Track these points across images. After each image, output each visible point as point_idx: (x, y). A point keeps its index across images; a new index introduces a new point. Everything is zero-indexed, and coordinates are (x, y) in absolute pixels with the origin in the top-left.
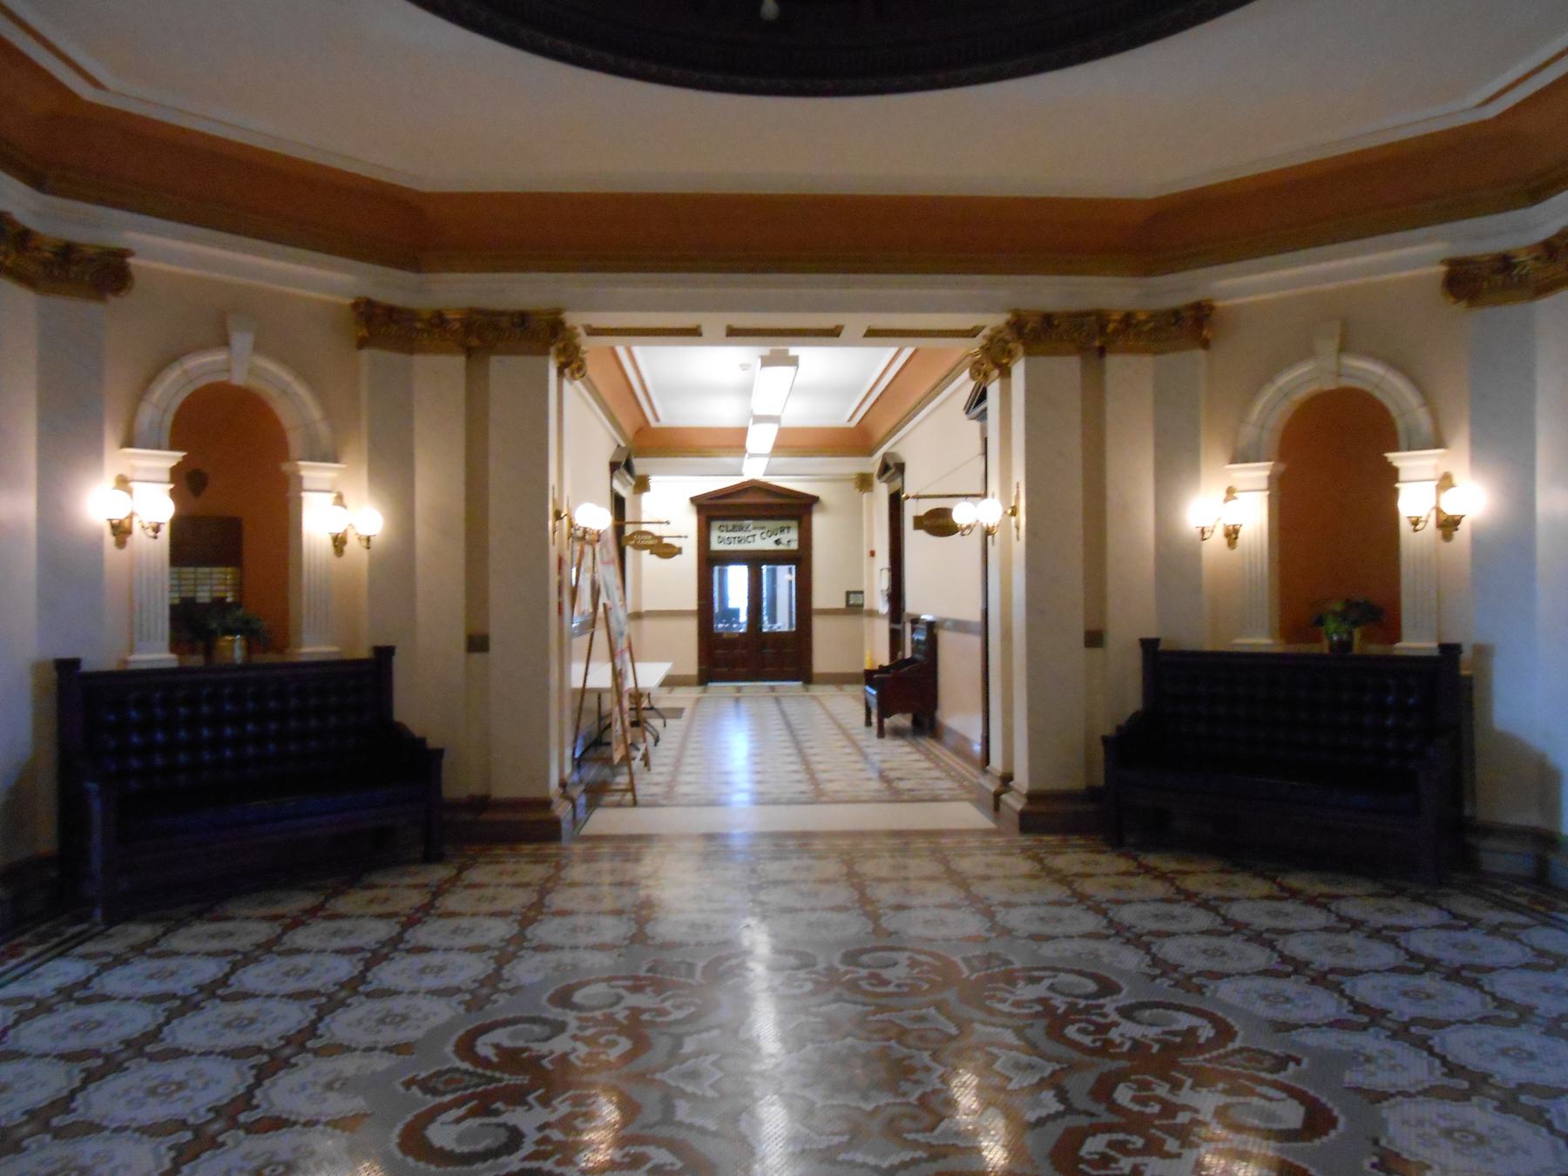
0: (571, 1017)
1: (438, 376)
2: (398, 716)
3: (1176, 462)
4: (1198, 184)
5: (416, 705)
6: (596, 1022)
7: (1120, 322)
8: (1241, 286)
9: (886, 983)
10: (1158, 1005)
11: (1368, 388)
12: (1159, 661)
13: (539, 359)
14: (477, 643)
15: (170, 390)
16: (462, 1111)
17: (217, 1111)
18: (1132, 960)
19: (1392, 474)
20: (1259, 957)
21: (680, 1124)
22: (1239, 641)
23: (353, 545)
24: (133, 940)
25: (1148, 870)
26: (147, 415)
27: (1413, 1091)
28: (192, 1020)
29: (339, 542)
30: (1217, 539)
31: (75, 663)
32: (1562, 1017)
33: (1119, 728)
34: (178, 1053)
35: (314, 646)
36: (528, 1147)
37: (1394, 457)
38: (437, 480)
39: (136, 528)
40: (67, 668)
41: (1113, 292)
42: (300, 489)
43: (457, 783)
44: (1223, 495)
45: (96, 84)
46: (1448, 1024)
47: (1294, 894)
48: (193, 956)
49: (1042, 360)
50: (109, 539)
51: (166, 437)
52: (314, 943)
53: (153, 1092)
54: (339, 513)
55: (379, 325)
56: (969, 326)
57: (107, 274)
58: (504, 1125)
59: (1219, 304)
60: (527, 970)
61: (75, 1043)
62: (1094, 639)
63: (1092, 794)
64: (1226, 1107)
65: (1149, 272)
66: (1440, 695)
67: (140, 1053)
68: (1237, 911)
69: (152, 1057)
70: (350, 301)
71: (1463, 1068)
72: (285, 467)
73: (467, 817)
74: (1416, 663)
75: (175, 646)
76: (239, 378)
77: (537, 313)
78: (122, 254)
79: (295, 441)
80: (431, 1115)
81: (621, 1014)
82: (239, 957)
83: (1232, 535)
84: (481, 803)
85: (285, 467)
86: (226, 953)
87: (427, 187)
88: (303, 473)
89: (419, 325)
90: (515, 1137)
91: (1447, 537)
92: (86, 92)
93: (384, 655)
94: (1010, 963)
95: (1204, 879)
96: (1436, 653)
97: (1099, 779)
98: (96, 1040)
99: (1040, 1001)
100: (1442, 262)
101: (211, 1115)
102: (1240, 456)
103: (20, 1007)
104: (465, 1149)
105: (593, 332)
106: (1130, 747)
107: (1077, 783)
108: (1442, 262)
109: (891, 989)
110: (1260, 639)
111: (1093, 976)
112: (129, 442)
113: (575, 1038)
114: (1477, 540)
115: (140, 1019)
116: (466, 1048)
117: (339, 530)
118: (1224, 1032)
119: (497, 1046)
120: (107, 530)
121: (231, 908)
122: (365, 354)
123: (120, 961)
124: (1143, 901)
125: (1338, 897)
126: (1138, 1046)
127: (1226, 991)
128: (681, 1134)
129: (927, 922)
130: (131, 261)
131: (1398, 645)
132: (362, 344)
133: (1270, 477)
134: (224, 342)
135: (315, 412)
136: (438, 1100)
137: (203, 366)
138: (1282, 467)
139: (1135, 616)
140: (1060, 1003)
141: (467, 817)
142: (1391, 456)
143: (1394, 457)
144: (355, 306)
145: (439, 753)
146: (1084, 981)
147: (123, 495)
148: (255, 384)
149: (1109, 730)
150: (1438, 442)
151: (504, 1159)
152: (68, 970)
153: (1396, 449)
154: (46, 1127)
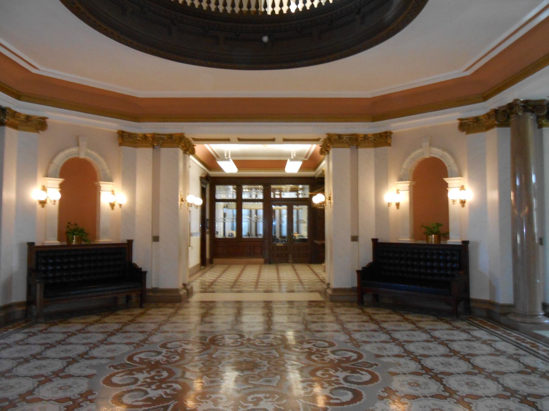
0: (164, 351)
1: (144, 154)
2: (135, 261)
3: (381, 182)
5: (139, 258)
6: (171, 352)
8: (397, 126)
9: (264, 343)
10: (345, 350)
12: (379, 247)
14: (156, 239)
15: (60, 160)
16: (123, 374)
17: (81, 395)
18: (343, 337)
19: (446, 185)
20: (442, 350)
21: (186, 378)
22: (401, 240)
23: (117, 207)
24: (40, 329)
25: (407, 320)
26: (52, 168)
27: (490, 395)
28: (76, 365)
29: (112, 205)
30: (393, 206)
31: (33, 243)
32: (547, 372)
33: (363, 268)
34: (70, 376)
35: (104, 239)
36: (139, 383)
37: (447, 180)
38: (143, 188)
39: (48, 201)
40: (31, 245)
42: (100, 190)
43: (151, 283)
44: (395, 191)
46: (505, 373)
47: (458, 328)
48: (58, 332)
50: (39, 206)
51: (58, 175)
52: (118, 341)
53: (60, 388)
54: (113, 196)
55: (125, 139)
58: (134, 378)
60: (157, 338)
61: (36, 372)
62: (355, 239)
64: (347, 376)
66: (459, 257)
67: (58, 376)
68: (437, 334)
69: (61, 377)
70: (116, 131)
71: (509, 388)
72: (96, 183)
73: (151, 294)
74: (454, 247)
75: (59, 239)
76: (82, 156)
77: (175, 134)
78: (44, 118)
80: (114, 375)
81: (179, 350)
82: (92, 345)
83: (398, 205)
84: (155, 290)
85: (96, 183)
86: (88, 344)
88: (101, 185)
89: (138, 138)
90: (137, 380)
91: (463, 206)
93: (130, 243)
94: (305, 338)
95: (427, 323)
96: (461, 244)
97: (355, 284)
98: (43, 372)
99: (309, 349)
101: (79, 396)
102: (401, 179)
103: (18, 361)
104: (121, 383)
105: (195, 140)
106: (366, 275)
107: (348, 286)
109: (265, 345)
110: (406, 239)
112: (47, 176)
113: (164, 356)
114: (471, 208)
115: (58, 365)
116: (130, 358)
117: (112, 202)
118: (360, 356)
119: (140, 358)
120: (38, 203)
121: (72, 320)
125: (419, 321)
126: (332, 361)
127: (368, 347)
128: (186, 381)
130: (47, 120)
132: (121, 144)
133: (410, 186)
135: (106, 167)
136: (117, 371)
137: (70, 152)
139: (369, 232)
140: (314, 349)
141: (151, 294)
142: (445, 179)
143: (447, 180)
145: (145, 273)
147: (44, 192)
149: (360, 269)
150: (460, 175)
151: (131, 386)
152: (19, 336)
153: (447, 177)
154: (24, 400)
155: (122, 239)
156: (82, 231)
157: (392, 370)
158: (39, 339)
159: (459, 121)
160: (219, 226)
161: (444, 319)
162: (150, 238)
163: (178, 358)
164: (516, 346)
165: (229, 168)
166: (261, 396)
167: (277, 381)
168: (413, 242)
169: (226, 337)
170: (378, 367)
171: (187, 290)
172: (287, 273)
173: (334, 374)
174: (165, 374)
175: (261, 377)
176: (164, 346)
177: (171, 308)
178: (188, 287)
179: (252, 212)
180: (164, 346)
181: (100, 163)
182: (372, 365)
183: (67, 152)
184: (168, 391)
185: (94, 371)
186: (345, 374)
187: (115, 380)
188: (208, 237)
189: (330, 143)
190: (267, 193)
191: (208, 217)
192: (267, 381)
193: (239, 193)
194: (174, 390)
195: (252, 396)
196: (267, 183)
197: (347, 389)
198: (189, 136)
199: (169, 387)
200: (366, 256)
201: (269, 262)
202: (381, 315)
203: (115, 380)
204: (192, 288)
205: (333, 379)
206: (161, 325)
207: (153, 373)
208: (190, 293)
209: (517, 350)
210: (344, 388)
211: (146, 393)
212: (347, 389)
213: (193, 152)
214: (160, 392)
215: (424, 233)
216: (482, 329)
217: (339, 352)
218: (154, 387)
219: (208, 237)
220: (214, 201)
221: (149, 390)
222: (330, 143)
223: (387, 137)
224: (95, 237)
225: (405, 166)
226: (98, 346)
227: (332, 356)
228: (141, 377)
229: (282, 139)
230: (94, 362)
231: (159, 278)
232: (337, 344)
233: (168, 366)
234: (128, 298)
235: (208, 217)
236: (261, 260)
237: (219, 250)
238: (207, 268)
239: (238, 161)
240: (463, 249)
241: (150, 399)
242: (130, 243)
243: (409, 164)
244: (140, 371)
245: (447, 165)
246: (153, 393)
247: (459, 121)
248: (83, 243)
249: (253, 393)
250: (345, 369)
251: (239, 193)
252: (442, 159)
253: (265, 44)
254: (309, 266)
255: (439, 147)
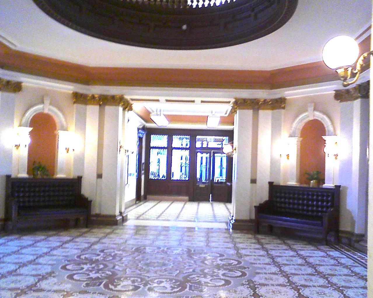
0: (102, 254)
1: (92, 110)
4: (281, 68)
5: (86, 190)
7: (263, 101)
8: (291, 94)
11: (320, 119)
13: (116, 107)
14: (100, 176)
18: (232, 252)
22: (289, 183)
35: (60, 175)
36: (84, 270)
40: (8, 177)
41: (261, 94)
43: (96, 210)
45: (15, 46)
48: (27, 240)
49: (241, 110)
51: (28, 125)
55: (79, 98)
56: (228, 101)
57: (17, 87)
59: (287, 98)
63: (251, 221)
65: (271, 89)
70: (72, 92)
73: (95, 218)
75: (28, 173)
76: (46, 111)
79: (58, 126)
80: (68, 265)
81: (113, 254)
84: (98, 215)
87: (91, 66)
90: (82, 268)
92: (13, 47)
93: (80, 179)
96: (334, 188)
97: (253, 217)
100: (334, 90)
105: (132, 100)
106: (262, 209)
108: (334, 90)
110: (293, 182)
111: (218, 254)
118: (239, 263)
122: (75, 105)
123: (11, 240)
124: (340, 275)
127: (247, 258)
129: (272, 279)
131: (324, 185)
132: (74, 103)
134: (42, 102)
135: (63, 120)
137: (38, 108)
138: (301, 139)
139: (264, 178)
141: (95, 218)
144: (73, 93)
145: (91, 201)
146: (217, 254)
148: (51, 113)
149: (258, 205)
155: (73, 175)
156: (44, 168)
157: (258, 271)
158: (16, 243)
159: (335, 92)
160: (153, 168)
161: (313, 244)
162: (95, 175)
163: (111, 258)
164: (354, 261)
165: (161, 122)
166: (163, 280)
167: (176, 274)
168: (298, 186)
169: (147, 248)
170: (250, 269)
171: (123, 217)
172: (205, 209)
173: (217, 272)
174: (101, 266)
175: (167, 271)
176: (102, 251)
177: (110, 228)
178: (124, 215)
179: (180, 158)
180: (102, 251)
181: (59, 117)
182: (245, 268)
183: (35, 108)
184: (103, 275)
185: (55, 262)
186: (224, 272)
187: (68, 267)
188: (143, 177)
189: (240, 104)
190: (193, 141)
191: (143, 161)
192: (169, 273)
193: (170, 141)
194: (107, 274)
195: (157, 280)
196: (193, 134)
197: (223, 279)
198: (127, 97)
199: (103, 273)
200: (265, 196)
201: (192, 199)
202: (264, 239)
203: (68, 267)
204: (127, 216)
205: (215, 274)
206: (101, 239)
207: (93, 265)
208: (124, 219)
209: (354, 263)
210: (220, 279)
211: (89, 275)
212: (223, 279)
213: (131, 109)
214: (98, 275)
215: (307, 178)
216: (336, 250)
217: (225, 260)
218: (94, 272)
219: (143, 177)
220: (149, 148)
221: (90, 274)
222: (240, 104)
223: (281, 102)
224: (53, 172)
225: (294, 125)
226: (46, 278)
227: (220, 262)
228: (86, 267)
229: (200, 102)
230: (55, 258)
231: (100, 207)
232: (226, 256)
233: (104, 262)
234: (77, 220)
235: (143, 161)
236: (187, 198)
237: (152, 189)
238: (141, 203)
239: (168, 115)
240: (336, 193)
241: (91, 278)
242: (80, 179)
243: (298, 124)
244: (86, 264)
245: (325, 126)
246: (93, 275)
247: (335, 92)
248: (45, 177)
249: (159, 278)
250: (225, 269)
251: (170, 141)
252: (322, 121)
253: (185, 31)
254: (225, 204)
255: (321, 111)
